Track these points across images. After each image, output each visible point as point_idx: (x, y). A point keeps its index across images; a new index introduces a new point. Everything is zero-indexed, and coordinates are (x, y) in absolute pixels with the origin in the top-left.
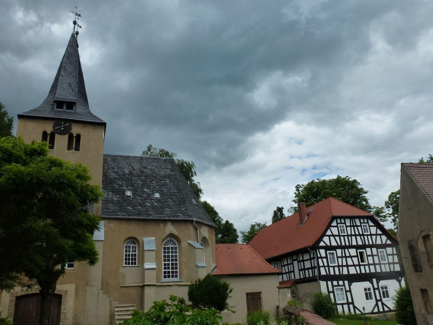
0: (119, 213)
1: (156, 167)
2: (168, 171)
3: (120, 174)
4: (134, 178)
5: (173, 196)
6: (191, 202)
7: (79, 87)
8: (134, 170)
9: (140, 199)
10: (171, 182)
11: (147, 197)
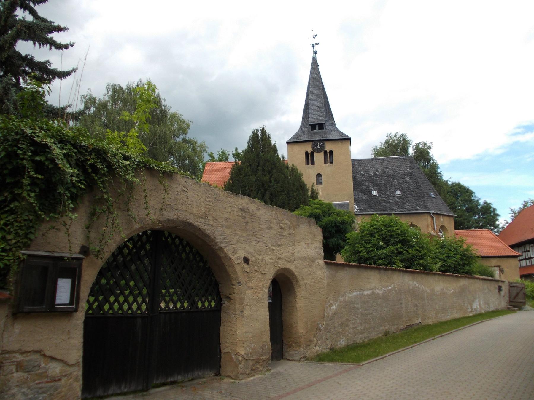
0: (368, 210)
1: (397, 166)
2: (408, 169)
3: (366, 176)
4: (378, 178)
5: (413, 192)
6: (430, 196)
7: (325, 108)
8: (377, 171)
9: (384, 196)
10: (410, 179)
11: (390, 195)
